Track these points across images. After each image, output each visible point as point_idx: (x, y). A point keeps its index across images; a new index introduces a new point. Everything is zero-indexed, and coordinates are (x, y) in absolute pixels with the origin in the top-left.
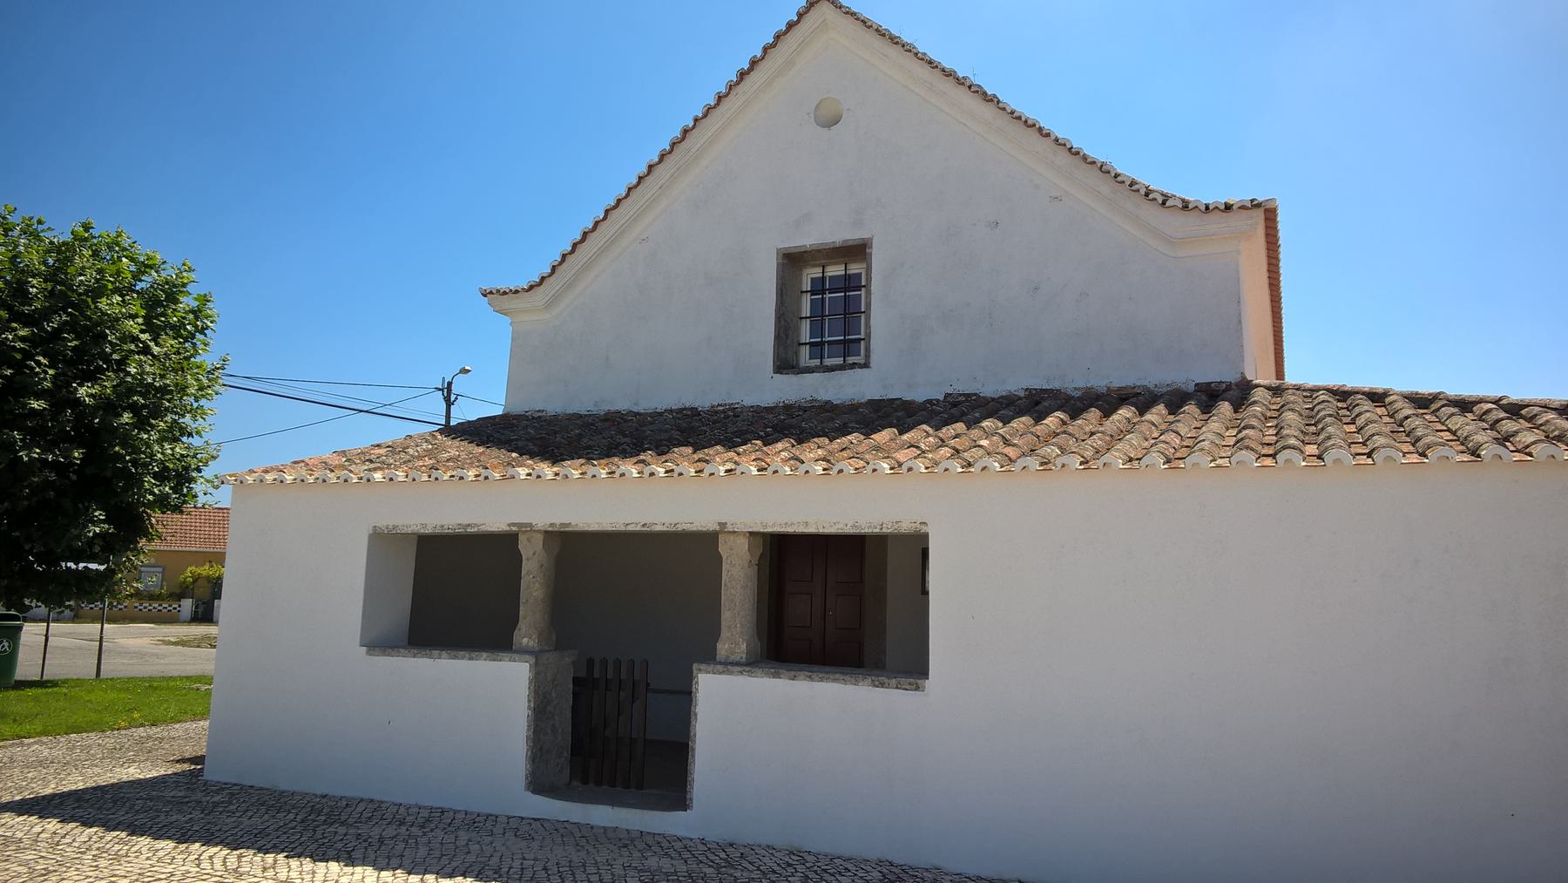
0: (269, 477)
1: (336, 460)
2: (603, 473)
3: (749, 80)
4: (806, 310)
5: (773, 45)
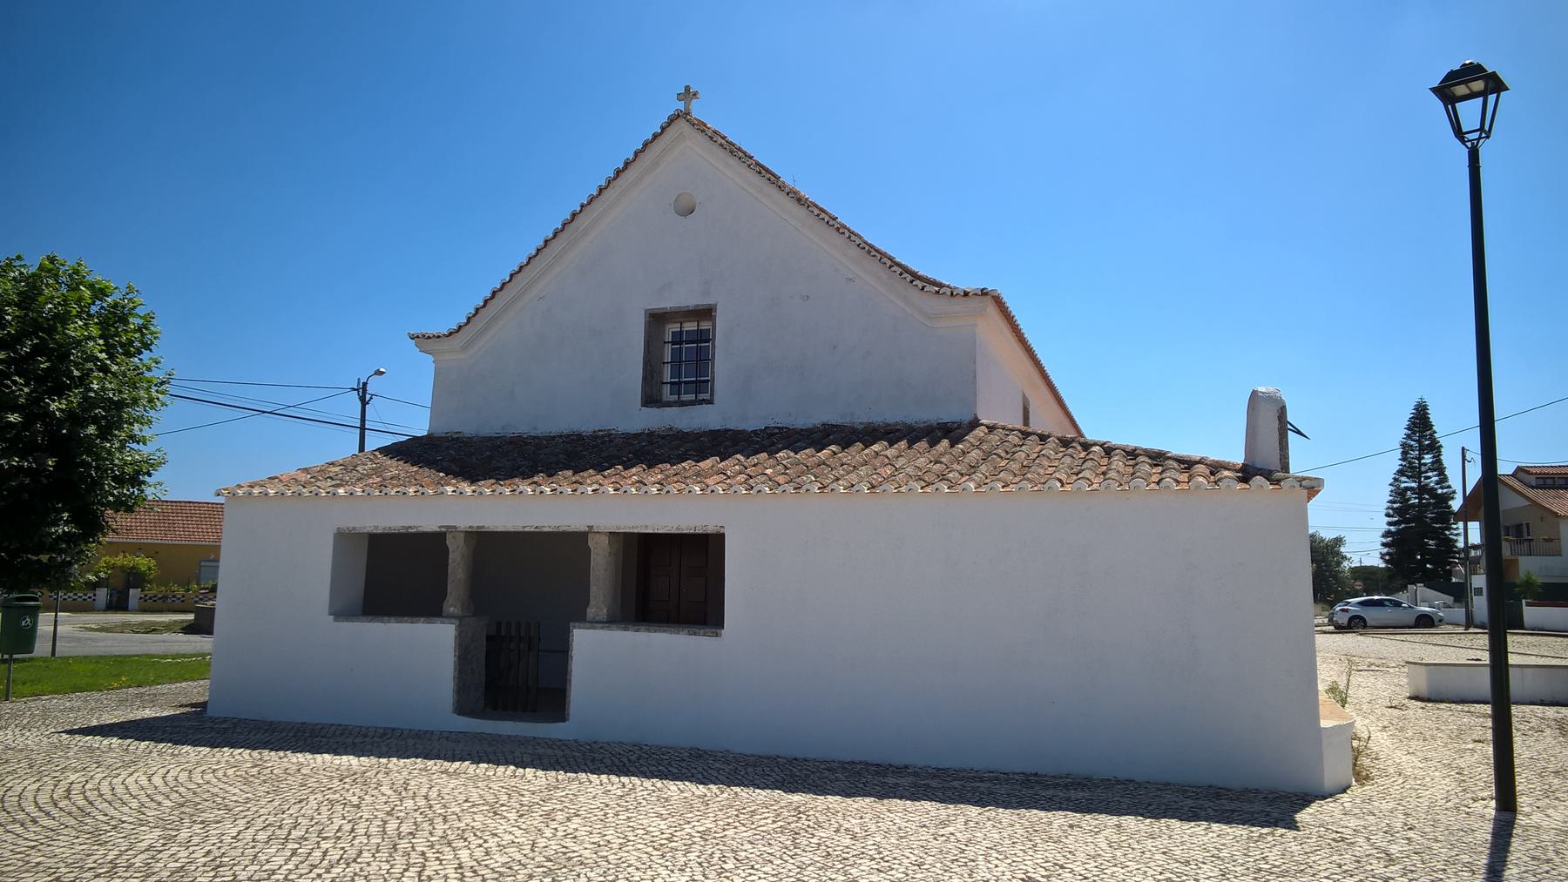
0: (256, 491)
1: (303, 477)
2: (507, 491)
3: (623, 176)
4: (668, 358)
5: (642, 151)
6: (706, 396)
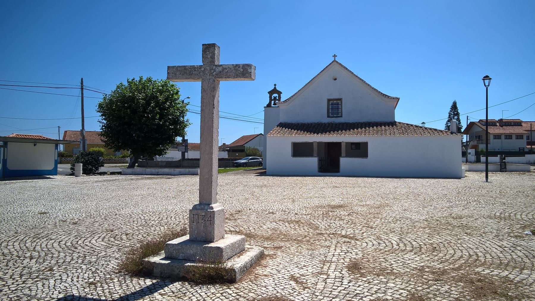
6: (340, 115)
